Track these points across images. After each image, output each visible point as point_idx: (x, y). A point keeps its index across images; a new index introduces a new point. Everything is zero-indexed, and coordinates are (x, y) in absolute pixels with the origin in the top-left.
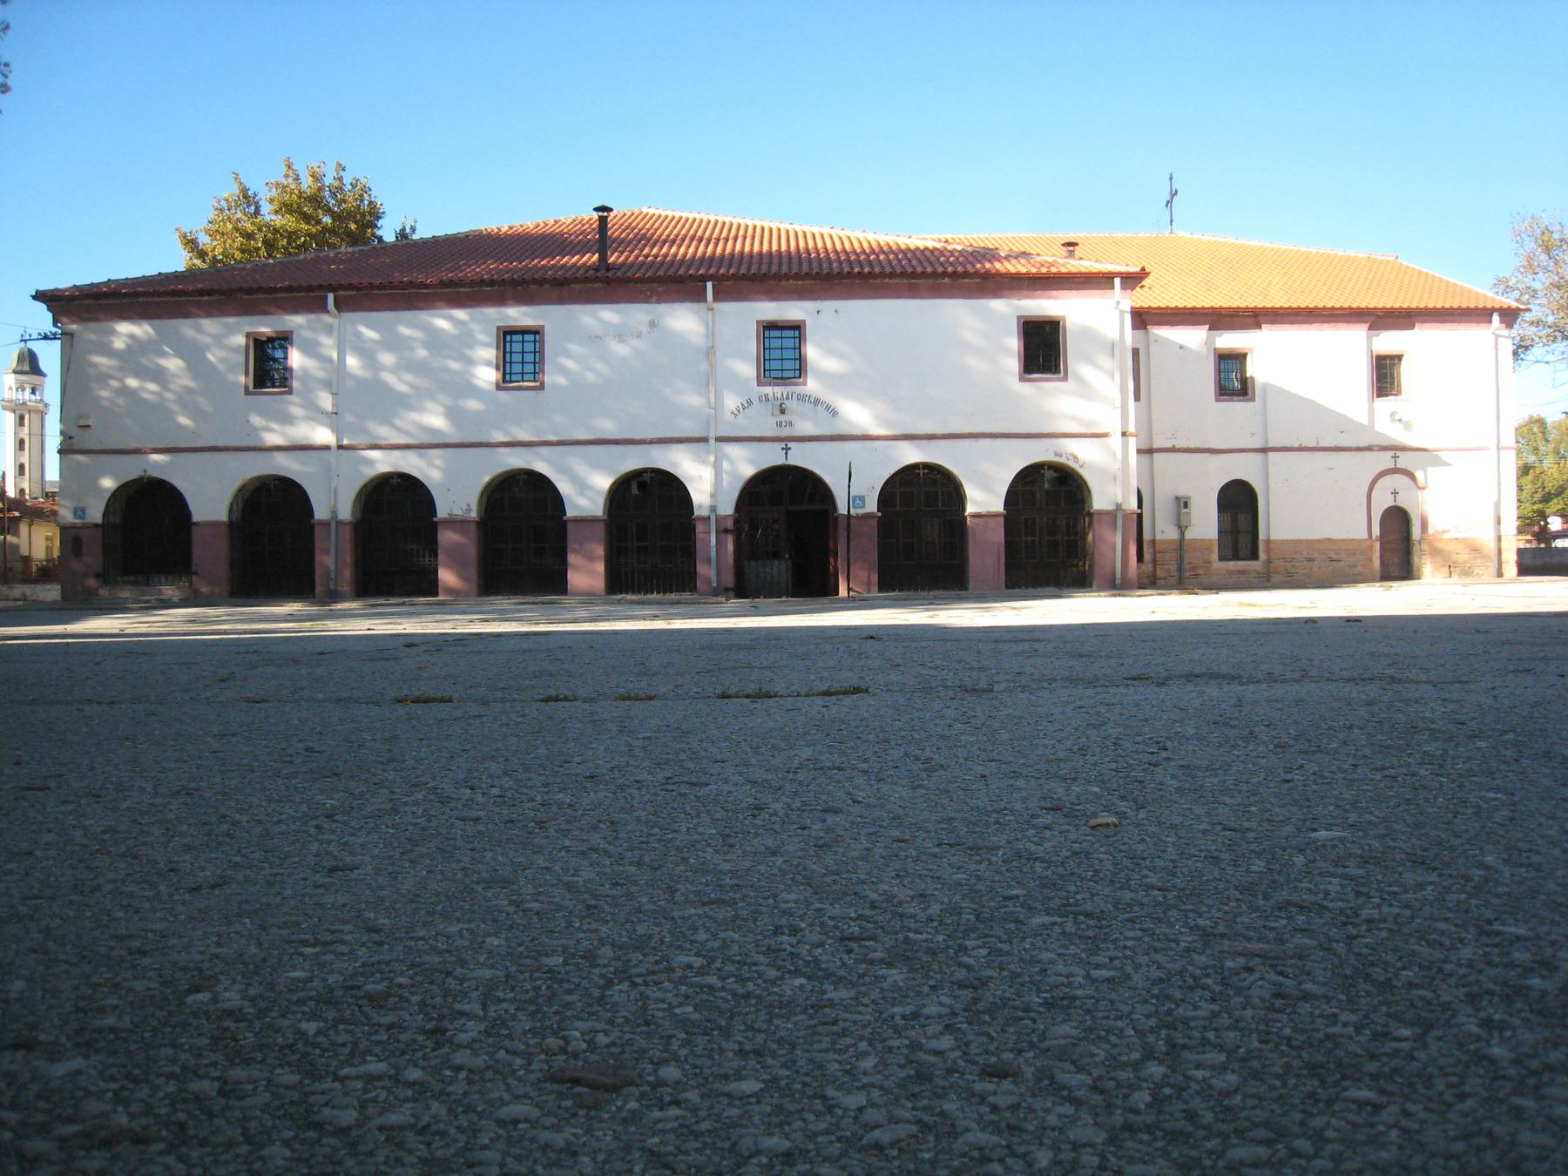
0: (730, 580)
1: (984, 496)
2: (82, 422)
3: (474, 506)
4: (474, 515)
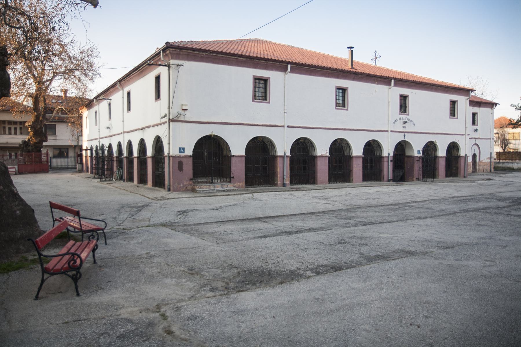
0: (391, 177)
1: (238, 148)
2: (184, 108)
3: (328, 152)
4: (244, 154)
